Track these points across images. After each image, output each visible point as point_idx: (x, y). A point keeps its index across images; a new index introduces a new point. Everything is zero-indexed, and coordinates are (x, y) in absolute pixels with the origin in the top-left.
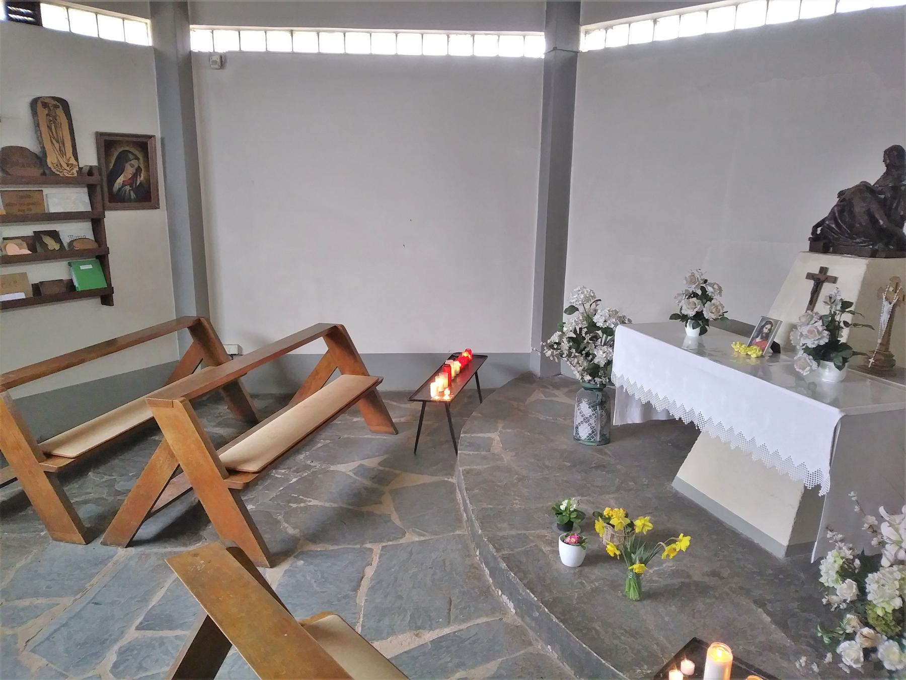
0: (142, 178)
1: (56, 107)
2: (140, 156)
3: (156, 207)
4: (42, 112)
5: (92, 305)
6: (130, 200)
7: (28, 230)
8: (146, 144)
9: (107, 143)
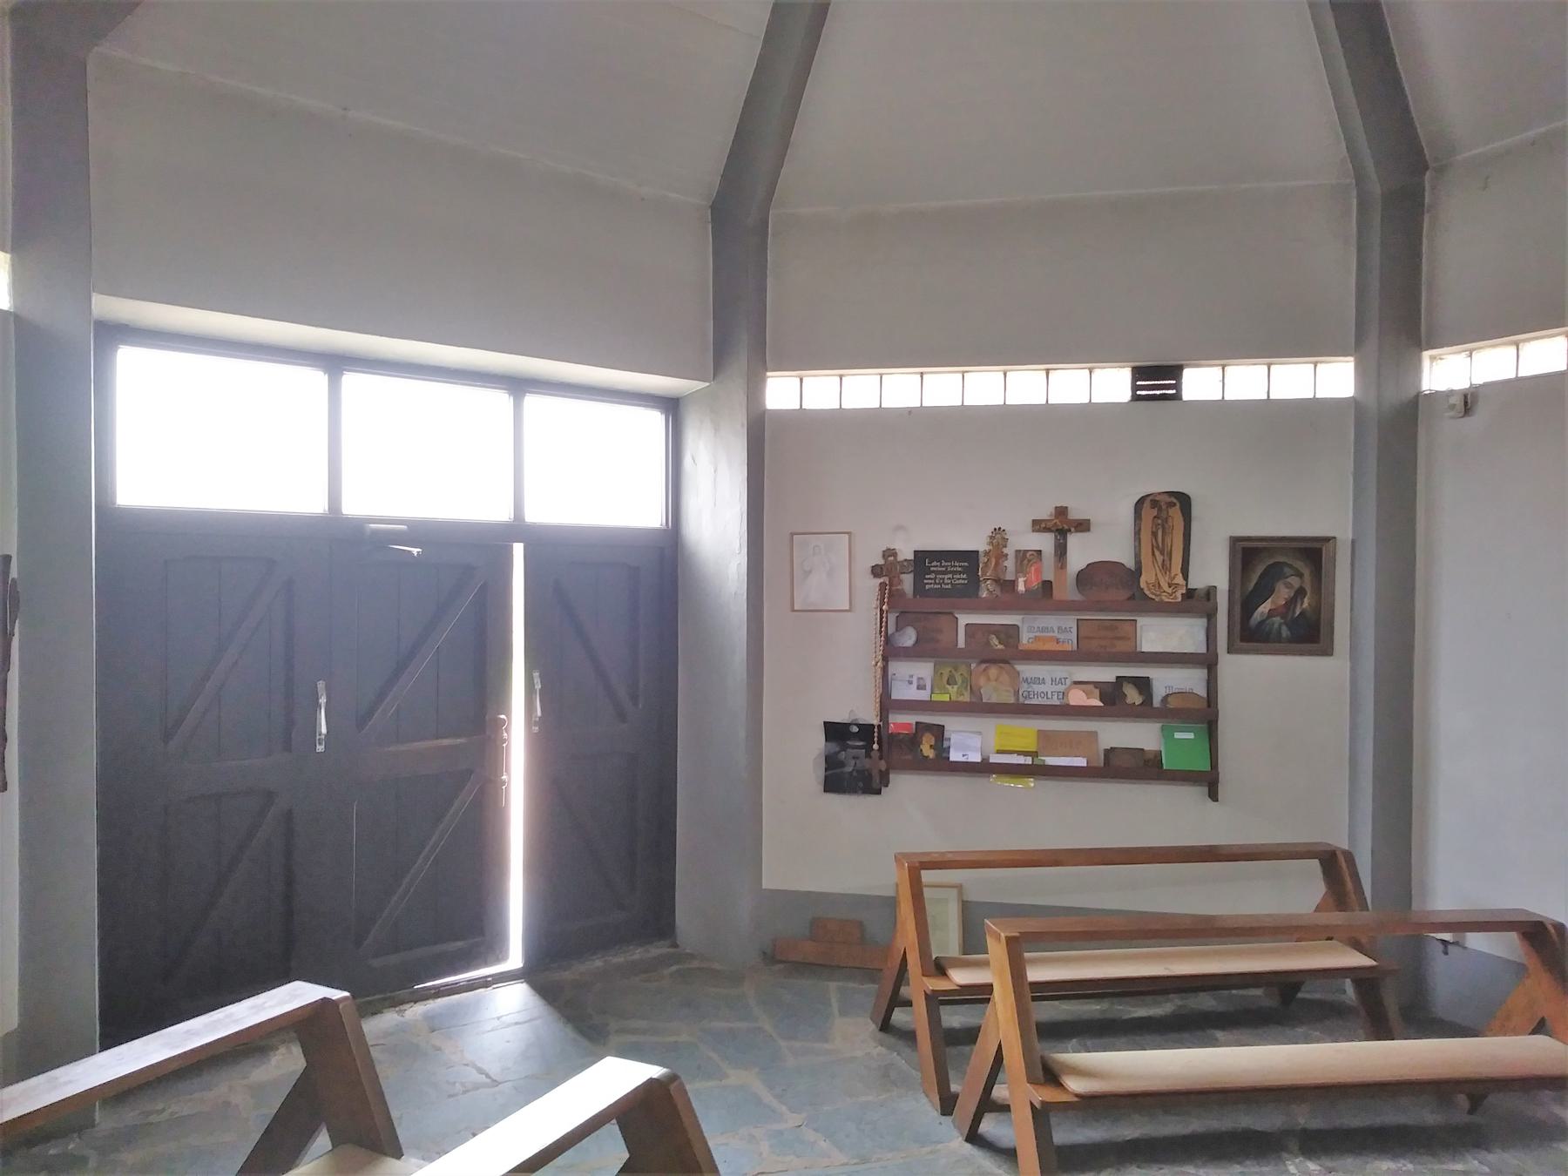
0: (1306, 605)
1: (1172, 505)
2: (1307, 573)
3: (1327, 651)
4: (1149, 513)
5: (1192, 795)
6: (1279, 639)
7: (1108, 674)
8: (1320, 550)
9: (1246, 553)
